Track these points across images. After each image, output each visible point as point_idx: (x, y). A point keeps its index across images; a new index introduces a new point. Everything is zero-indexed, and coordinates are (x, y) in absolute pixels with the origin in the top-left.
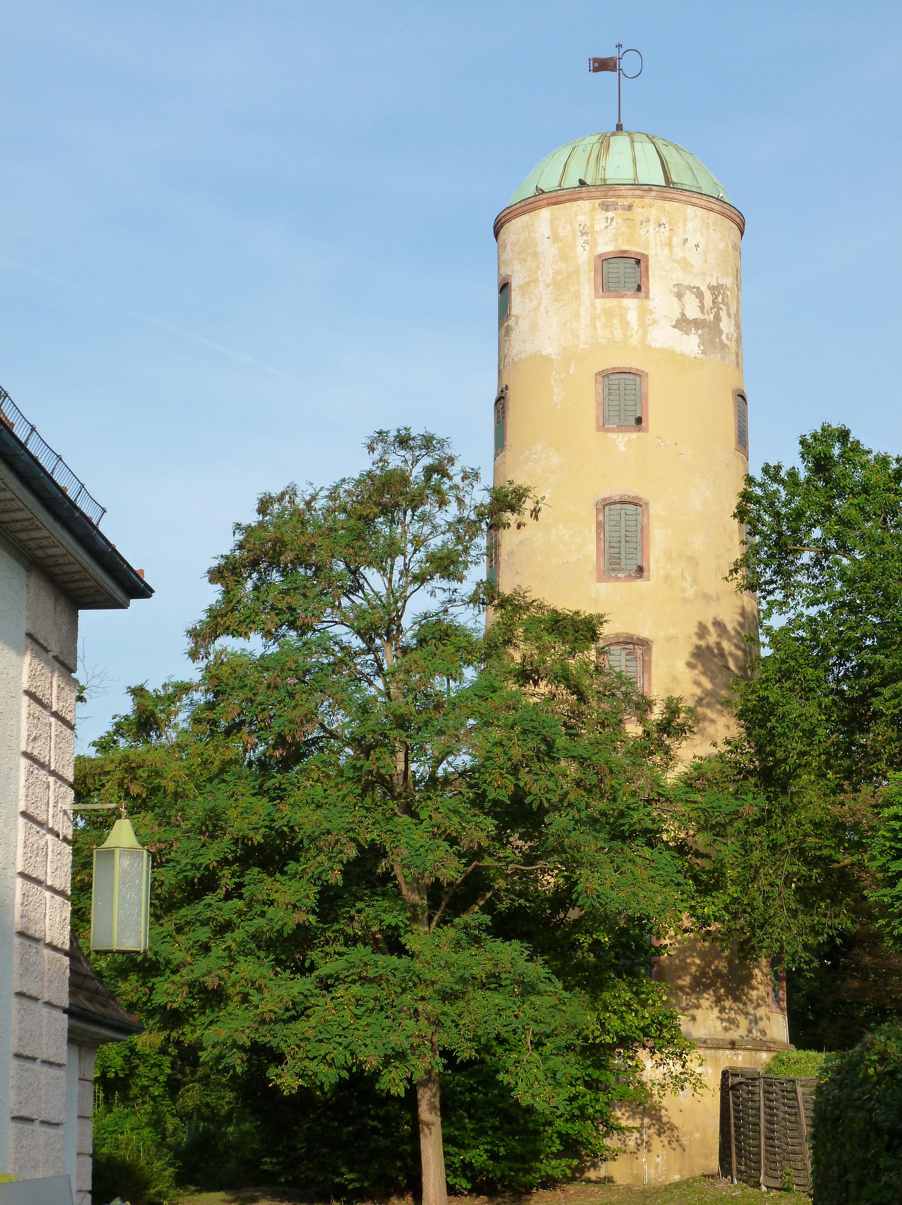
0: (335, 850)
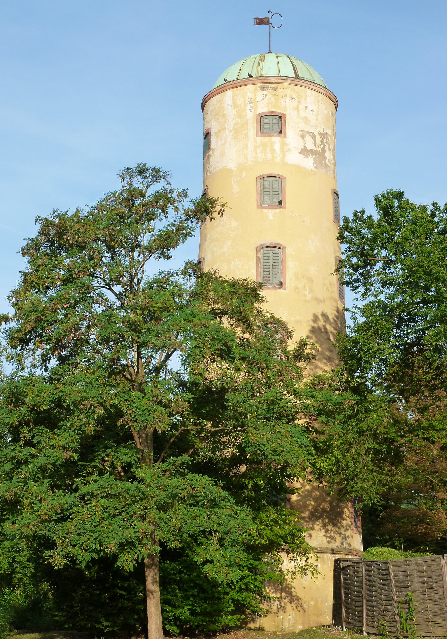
0: (90, 411)
